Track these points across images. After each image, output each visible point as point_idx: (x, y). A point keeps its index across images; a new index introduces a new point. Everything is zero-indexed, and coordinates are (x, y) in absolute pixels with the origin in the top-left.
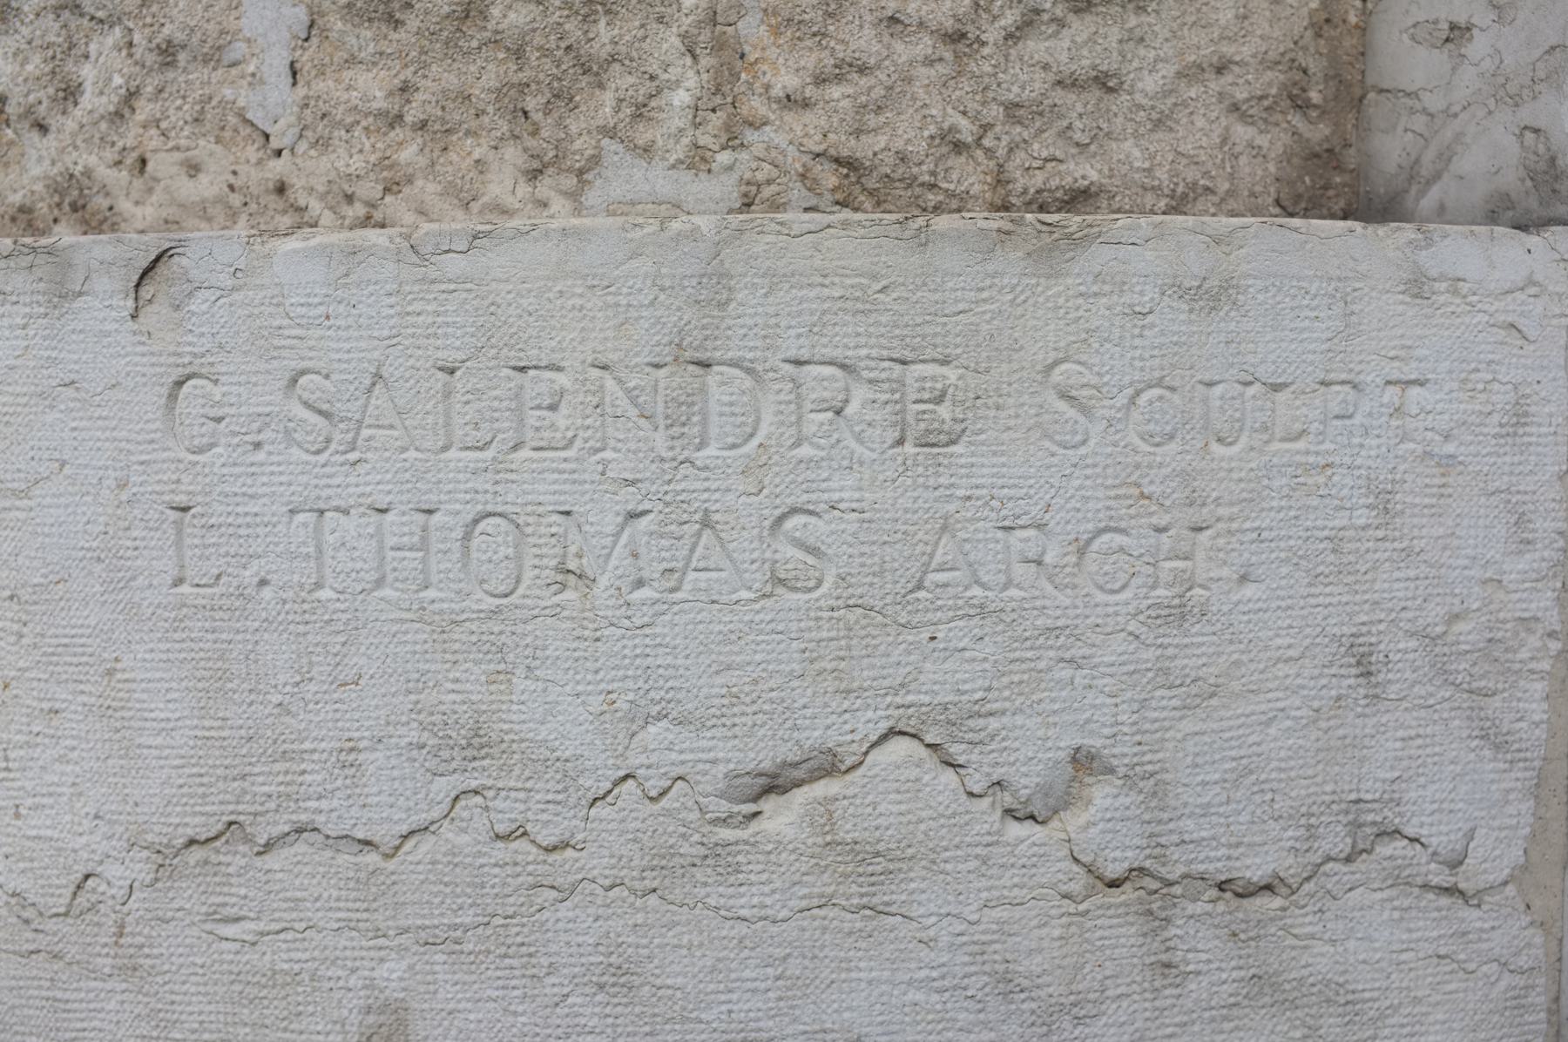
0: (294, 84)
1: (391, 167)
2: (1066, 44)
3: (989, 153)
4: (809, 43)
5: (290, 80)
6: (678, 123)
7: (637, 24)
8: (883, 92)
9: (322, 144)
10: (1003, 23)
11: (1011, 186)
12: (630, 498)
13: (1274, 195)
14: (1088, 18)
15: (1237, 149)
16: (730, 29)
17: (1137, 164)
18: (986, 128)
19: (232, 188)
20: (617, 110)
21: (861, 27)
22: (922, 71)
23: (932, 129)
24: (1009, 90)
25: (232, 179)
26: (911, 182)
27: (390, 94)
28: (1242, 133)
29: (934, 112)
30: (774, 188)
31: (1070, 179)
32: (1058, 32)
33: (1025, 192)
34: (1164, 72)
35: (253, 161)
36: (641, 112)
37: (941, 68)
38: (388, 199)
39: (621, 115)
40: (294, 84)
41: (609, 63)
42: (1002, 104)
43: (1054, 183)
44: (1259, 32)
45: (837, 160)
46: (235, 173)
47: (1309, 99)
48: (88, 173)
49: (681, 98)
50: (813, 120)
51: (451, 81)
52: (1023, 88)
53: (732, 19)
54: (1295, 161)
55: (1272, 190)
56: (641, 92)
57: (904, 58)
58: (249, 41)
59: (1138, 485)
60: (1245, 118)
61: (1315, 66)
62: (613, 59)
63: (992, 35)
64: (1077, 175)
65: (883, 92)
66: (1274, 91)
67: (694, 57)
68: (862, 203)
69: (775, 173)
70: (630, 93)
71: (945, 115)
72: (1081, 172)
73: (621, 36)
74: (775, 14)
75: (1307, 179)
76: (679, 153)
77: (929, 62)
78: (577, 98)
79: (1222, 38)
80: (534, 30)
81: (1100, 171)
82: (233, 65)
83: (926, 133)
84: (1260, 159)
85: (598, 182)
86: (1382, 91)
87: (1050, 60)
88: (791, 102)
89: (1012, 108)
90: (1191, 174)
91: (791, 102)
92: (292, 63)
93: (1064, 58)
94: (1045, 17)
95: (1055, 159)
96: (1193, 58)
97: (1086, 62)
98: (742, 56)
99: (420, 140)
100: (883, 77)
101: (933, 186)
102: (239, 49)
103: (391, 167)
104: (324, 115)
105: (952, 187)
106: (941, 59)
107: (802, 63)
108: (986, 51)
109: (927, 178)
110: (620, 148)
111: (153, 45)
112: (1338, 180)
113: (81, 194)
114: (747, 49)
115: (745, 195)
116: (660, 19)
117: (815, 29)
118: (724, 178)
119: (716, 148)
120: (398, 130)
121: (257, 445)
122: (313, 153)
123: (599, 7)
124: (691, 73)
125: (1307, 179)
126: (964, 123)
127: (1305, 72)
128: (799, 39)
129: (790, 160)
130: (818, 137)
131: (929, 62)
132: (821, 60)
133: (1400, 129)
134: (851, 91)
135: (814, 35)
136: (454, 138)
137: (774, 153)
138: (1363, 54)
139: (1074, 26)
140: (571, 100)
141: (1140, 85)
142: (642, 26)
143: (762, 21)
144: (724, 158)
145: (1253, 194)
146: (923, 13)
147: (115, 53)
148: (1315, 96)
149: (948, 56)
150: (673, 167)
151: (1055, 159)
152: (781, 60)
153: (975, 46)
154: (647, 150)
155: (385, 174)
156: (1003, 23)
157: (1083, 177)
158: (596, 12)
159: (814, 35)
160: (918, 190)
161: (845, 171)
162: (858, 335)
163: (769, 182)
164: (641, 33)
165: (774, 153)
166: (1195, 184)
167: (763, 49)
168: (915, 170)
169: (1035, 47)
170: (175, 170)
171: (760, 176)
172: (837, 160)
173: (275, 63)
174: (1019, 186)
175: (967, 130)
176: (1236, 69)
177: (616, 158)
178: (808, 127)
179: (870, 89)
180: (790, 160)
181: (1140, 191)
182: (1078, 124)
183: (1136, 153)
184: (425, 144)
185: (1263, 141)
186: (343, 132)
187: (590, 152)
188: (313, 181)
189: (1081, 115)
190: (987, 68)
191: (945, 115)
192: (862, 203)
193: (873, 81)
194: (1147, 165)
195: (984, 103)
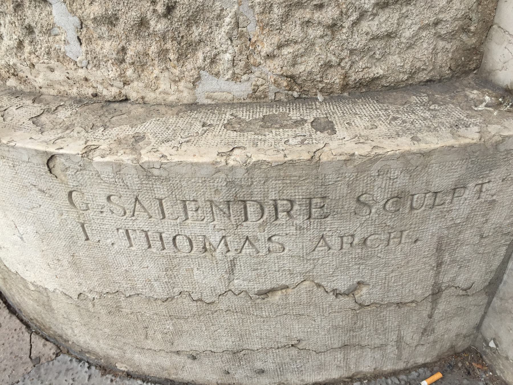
0: (81, 44)
1: (124, 77)
2: (377, 22)
3: (343, 68)
4: (275, 32)
5: (79, 43)
6: (227, 65)
7: (208, 27)
8: (304, 51)
9: (97, 66)
10: (352, 19)
11: (350, 78)
12: (224, 233)
13: (449, 66)
14: (387, 10)
15: (438, 51)
16: (244, 29)
17: (398, 65)
18: (342, 60)
19: (68, 78)
20: (205, 60)
21: (296, 26)
22: (319, 40)
23: (322, 62)
24: (352, 45)
25: (67, 75)
26: (313, 81)
27: (118, 53)
28: (441, 44)
29: (323, 57)
30: (264, 87)
31: (372, 75)
32: (374, 18)
33: (355, 80)
34: (414, 29)
35: (73, 69)
36: (213, 61)
37: (326, 38)
38: (126, 87)
39: (206, 63)
40: (81, 44)
41: (199, 43)
42: (349, 49)
43: (366, 76)
44: (455, 8)
45: (287, 77)
46: (68, 73)
47: (470, 30)
48: (15, 65)
49: (228, 56)
50: (277, 62)
51: (140, 48)
52: (358, 44)
53: (245, 25)
54: (460, 51)
55: (448, 64)
56: (213, 54)
57: (312, 37)
58: (59, 27)
59: (385, 223)
60: (443, 39)
61: (474, 16)
62: (200, 41)
63: (347, 24)
64: (375, 73)
65: (304, 51)
66: (457, 28)
67: (231, 41)
68: (295, 89)
69: (264, 82)
70: (208, 54)
71: (327, 57)
72: (377, 71)
73: (202, 32)
74: (261, 22)
75: (463, 58)
76: (229, 75)
77: (322, 37)
78: (189, 56)
79: (440, 12)
80: (169, 31)
81: (384, 70)
82: (56, 35)
83: (320, 64)
84: (446, 52)
85: (200, 85)
86: (499, 27)
87: (369, 30)
88: (269, 56)
89: (352, 52)
90: (418, 64)
91: (269, 56)
92: (78, 37)
93: (374, 29)
94: (369, 13)
95: (367, 67)
96: (427, 22)
97: (383, 30)
98: (250, 40)
99: (133, 68)
100: (304, 45)
101: (321, 82)
102: (56, 31)
103: (124, 77)
104: (95, 58)
105: (328, 81)
106: (326, 35)
107: (273, 41)
108: (344, 30)
109: (319, 79)
110: (208, 74)
111: (23, 27)
112: (475, 58)
113: (15, 71)
114: (252, 37)
115: (254, 90)
116: (217, 25)
117: (277, 28)
118: (246, 83)
119: (242, 74)
120: (124, 64)
121: (102, 212)
122: (94, 69)
123: (193, 21)
124: (230, 47)
125: (463, 58)
126: (333, 58)
127: (470, 19)
128: (271, 31)
129: (269, 77)
130: (279, 69)
131: (322, 37)
132: (280, 40)
133: (504, 46)
134: (292, 51)
135: (277, 29)
136: (146, 67)
137: (263, 75)
138: (495, 9)
139: (380, 15)
140: (186, 56)
141: (404, 35)
142: (210, 28)
143: (257, 25)
144: (245, 77)
145: (441, 67)
146: (320, 19)
147: (10, 25)
148: (472, 28)
149: (329, 33)
150: (227, 80)
151: (367, 67)
152: (265, 40)
153: (340, 28)
154: (217, 75)
155: (122, 79)
156: (352, 19)
157: (377, 73)
158: (192, 23)
159: (277, 29)
160: (315, 83)
161: (289, 79)
162: (295, 192)
163: (262, 85)
164: (210, 31)
165: (263, 75)
166: (419, 68)
167: (258, 36)
168: (315, 77)
169: (365, 26)
170: (46, 69)
171: (259, 83)
172: (287, 77)
173: (72, 36)
174: (353, 79)
175: (334, 60)
176: (443, 23)
177: (206, 77)
178: (274, 65)
179: (299, 50)
180: (269, 77)
181: (398, 73)
182: (378, 52)
183: (399, 60)
184: (135, 69)
185: (448, 46)
186: (104, 63)
187: (196, 76)
188: (97, 79)
189: (379, 49)
190: (344, 37)
191: (327, 57)
192: (295, 89)
193: (300, 47)
194: (402, 64)
195: (342, 51)
